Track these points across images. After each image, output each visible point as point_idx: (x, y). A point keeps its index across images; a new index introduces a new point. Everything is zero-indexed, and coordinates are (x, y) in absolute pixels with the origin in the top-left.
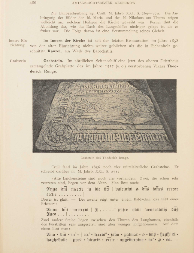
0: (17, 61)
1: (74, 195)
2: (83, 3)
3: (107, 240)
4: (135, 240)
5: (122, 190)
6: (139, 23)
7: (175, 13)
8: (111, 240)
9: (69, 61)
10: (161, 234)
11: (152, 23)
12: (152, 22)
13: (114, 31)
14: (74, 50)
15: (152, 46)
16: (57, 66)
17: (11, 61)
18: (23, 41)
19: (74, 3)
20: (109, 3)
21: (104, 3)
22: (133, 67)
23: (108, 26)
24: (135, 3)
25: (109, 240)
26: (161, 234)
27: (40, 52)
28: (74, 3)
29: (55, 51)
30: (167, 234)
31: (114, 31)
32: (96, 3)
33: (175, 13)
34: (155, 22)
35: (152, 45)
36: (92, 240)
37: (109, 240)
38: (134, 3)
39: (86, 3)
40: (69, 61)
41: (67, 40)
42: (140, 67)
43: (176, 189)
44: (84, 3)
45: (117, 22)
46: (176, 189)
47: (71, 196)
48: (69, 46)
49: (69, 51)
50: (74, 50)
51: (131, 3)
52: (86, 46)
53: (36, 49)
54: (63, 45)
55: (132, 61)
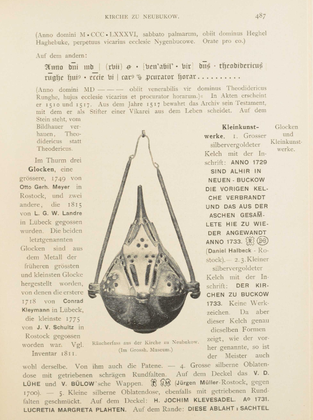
0: (261, 312)
1: (232, 78)
3: (92, 78)
4: (167, 77)
5: (157, 79)
6: (247, 189)
7: (42, 36)
8: (98, 78)
10: (70, 78)
11: (245, 331)
12: (246, 329)
13: (257, 304)
17: (246, 137)
23: (188, 111)
25: (95, 78)
26: (70, 78)
30: (56, 77)
31: (257, 304)
33: (42, 36)
34: (81, 56)
36: (160, 78)
37: (95, 78)
38: (175, 16)
41: (229, 127)
43: (186, 77)
46: (186, 77)
47: (219, 78)
53: (217, 107)
55: (37, 240)
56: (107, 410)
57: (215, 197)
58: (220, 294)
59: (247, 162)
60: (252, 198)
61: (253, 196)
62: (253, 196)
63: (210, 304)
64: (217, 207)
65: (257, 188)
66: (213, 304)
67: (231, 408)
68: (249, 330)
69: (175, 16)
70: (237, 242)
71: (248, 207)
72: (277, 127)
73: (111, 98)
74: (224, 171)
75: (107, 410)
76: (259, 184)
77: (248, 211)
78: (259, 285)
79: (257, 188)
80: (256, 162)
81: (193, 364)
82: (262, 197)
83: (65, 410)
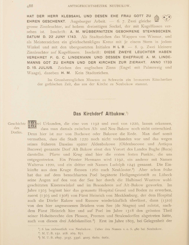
2: (78, 6)
9: (86, 53)
14: (28, 72)
15: (166, 165)
16: (116, 191)
18: (102, 221)
19: (70, 6)
20: (104, 6)
21: (99, 6)
22: (117, 155)
24: (129, 6)
27: (41, 185)
28: (70, 6)
29: (151, 190)
32: (91, 6)
35: (166, 164)
38: (128, 6)
39: (82, 6)
40: (86, 53)
42: (165, 190)
44: (80, 6)
45: (148, 21)
48: (52, 42)
49: (113, 84)
50: (146, 179)
51: (125, 6)
52: (138, 160)
54: (32, 46)
56: (140, 62)
57: (109, 62)
58: (105, 16)
59: (159, 62)
60: (85, 57)
61: (86, 56)
62: (86, 56)
63: (165, 62)
64: (84, 62)
65: (165, 31)
66: (167, 62)
67: (143, 62)
68: (117, 150)
69: (128, 6)
70: (170, 62)
71: (50, 68)
72: (56, 80)
73: (157, 62)
74: (84, 62)
75: (140, 62)
76: (169, 152)
77: (96, 142)
78: (101, 62)
79: (165, 31)
80: (165, 62)
81: (145, 220)
82: (49, 62)
83: (139, 62)
